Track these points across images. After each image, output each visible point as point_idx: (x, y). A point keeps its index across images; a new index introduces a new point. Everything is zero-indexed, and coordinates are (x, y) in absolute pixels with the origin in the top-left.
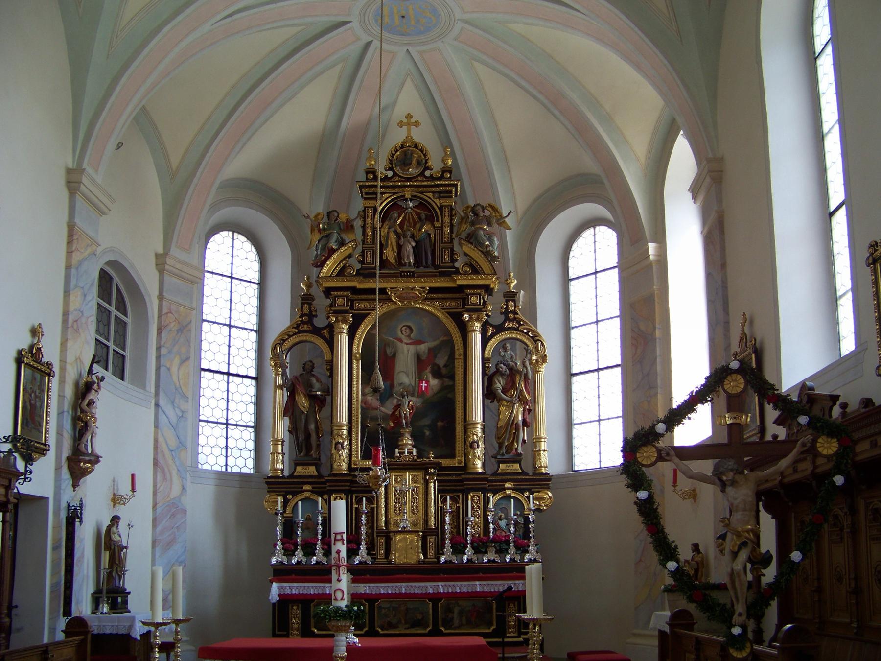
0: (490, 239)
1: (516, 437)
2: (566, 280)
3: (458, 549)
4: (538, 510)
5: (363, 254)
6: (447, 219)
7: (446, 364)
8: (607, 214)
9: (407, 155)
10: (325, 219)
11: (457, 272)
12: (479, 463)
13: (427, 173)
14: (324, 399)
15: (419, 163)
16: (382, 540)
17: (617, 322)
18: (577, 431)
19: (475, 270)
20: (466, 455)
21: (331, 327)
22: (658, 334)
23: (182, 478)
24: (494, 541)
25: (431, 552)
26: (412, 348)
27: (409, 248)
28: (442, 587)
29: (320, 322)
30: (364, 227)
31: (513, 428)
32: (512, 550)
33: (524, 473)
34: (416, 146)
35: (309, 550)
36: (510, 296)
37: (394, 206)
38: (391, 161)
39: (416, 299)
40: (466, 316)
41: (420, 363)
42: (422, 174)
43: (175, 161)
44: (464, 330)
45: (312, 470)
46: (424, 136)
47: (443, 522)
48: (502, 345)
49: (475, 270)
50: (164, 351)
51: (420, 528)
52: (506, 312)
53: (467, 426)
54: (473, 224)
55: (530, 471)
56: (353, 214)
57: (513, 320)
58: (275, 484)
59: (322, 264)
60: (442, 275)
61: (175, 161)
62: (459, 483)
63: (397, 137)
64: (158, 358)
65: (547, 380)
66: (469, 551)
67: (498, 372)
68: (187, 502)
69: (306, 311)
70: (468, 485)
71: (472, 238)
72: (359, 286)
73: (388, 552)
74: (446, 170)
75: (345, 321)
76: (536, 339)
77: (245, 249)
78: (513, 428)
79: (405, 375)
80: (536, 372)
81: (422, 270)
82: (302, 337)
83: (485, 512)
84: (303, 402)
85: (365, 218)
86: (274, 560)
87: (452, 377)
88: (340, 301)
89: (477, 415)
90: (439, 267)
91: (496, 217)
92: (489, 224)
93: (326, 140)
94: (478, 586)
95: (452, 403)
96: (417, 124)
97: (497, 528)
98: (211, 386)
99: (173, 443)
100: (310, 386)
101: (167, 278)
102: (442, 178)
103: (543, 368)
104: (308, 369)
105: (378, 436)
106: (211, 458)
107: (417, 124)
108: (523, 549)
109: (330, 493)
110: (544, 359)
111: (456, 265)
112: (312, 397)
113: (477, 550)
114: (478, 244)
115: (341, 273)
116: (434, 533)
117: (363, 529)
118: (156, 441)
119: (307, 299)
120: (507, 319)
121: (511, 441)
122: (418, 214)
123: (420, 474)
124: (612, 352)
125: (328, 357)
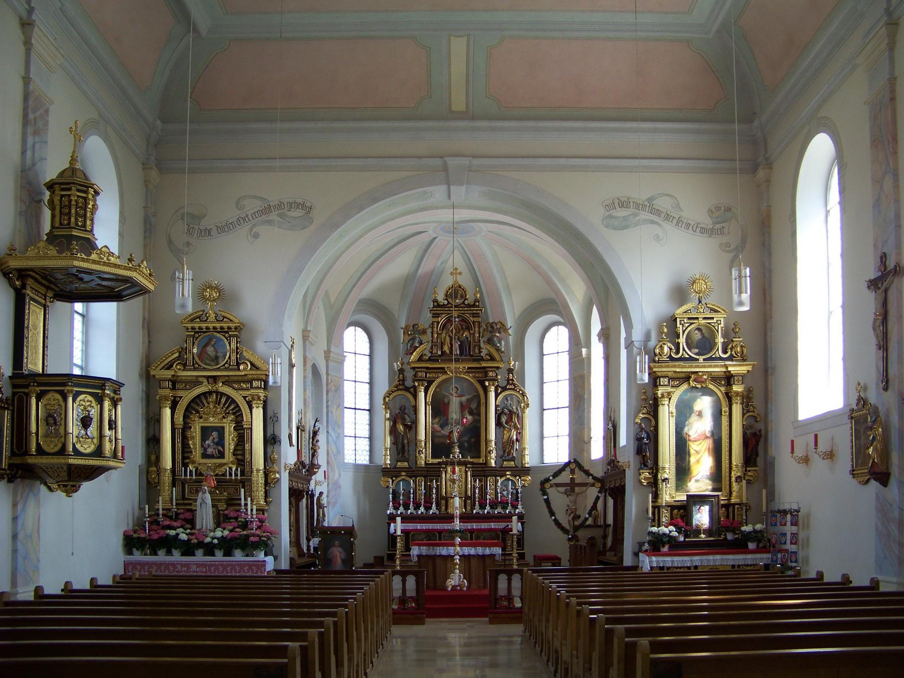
0: (500, 342)
1: (512, 447)
2: (542, 355)
3: (483, 507)
4: (523, 486)
5: (432, 348)
6: (477, 329)
7: (475, 407)
8: (561, 319)
9: (456, 291)
10: (411, 328)
11: (482, 359)
12: (493, 462)
13: (466, 302)
14: (412, 426)
15: (462, 297)
16: (443, 502)
17: (567, 382)
18: (545, 441)
19: (492, 359)
20: (486, 457)
21: (415, 387)
22: (586, 396)
23: (339, 470)
24: (500, 502)
25: (469, 508)
26: (458, 399)
27: (456, 346)
28: (475, 526)
29: (409, 383)
30: (432, 333)
31: (511, 442)
32: (510, 507)
33: (516, 467)
34: (460, 287)
35: (407, 507)
36: (510, 371)
37: (449, 321)
38: (446, 295)
39: (460, 373)
40: (487, 383)
41: (462, 407)
42: (463, 303)
43: (333, 299)
44: (486, 390)
45: (406, 464)
46: (465, 280)
47: (475, 492)
48: (506, 398)
49: (492, 359)
50: (330, 403)
51: (463, 495)
52: (508, 380)
53: (487, 442)
54: (491, 332)
55: (520, 466)
56: (427, 326)
57: (512, 384)
58: (390, 472)
59: (412, 354)
60: (474, 360)
61: (333, 299)
62: (482, 472)
63: (448, 282)
64: (327, 407)
65: (530, 417)
66: (488, 507)
67: (503, 412)
68: (341, 482)
69: (401, 378)
70: (487, 473)
71: (490, 341)
72: (430, 366)
73: (447, 508)
74: (476, 301)
75: (422, 385)
76: (523, 395)
77: (361, 334)
78: (511, 442)
79: (454, 413)
80: (523, 412)
81: (463, 357)
82: (400, 392)
83: (497, 487)
84: (401, 428)
85: (433, 328)
86: (388, 512)
87: (479, 415)
88: (420, 374)
89: (492, 436)
90: (472, 356)
91: (503, 328)
92: (499, 333)
93: (408, 280)
94: (493, 525)
95: (479, 428)
96: (460, 273)
97: (502, 495)
98: (348, 415)
99: (335, 451)
100: (404, 419)
101: (330, 364)
102: (474, 306)
103: (527, 411)
104: (403, 409)
105: (440, 448)
106: (349, 458)
107: (460, 273)
108: (515, 507)
109: (416, 477)
110: (528, 405)
111: (482, 354)
112: (405, 426)
113: (492, 507)
114: (494, 345)
115: (420, 359)
116: (470, 498)
117: (434, 496)
118: (328, 451)
119: (401, 371)
120: (508, 383)
121: (507, 448)
122: (462, 326)
123: (463, 468)
124: (565, 400)
125: (413, 403)
